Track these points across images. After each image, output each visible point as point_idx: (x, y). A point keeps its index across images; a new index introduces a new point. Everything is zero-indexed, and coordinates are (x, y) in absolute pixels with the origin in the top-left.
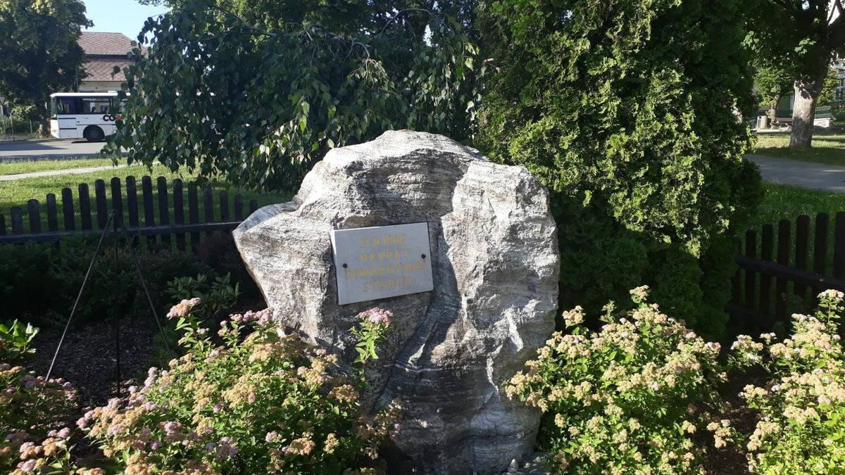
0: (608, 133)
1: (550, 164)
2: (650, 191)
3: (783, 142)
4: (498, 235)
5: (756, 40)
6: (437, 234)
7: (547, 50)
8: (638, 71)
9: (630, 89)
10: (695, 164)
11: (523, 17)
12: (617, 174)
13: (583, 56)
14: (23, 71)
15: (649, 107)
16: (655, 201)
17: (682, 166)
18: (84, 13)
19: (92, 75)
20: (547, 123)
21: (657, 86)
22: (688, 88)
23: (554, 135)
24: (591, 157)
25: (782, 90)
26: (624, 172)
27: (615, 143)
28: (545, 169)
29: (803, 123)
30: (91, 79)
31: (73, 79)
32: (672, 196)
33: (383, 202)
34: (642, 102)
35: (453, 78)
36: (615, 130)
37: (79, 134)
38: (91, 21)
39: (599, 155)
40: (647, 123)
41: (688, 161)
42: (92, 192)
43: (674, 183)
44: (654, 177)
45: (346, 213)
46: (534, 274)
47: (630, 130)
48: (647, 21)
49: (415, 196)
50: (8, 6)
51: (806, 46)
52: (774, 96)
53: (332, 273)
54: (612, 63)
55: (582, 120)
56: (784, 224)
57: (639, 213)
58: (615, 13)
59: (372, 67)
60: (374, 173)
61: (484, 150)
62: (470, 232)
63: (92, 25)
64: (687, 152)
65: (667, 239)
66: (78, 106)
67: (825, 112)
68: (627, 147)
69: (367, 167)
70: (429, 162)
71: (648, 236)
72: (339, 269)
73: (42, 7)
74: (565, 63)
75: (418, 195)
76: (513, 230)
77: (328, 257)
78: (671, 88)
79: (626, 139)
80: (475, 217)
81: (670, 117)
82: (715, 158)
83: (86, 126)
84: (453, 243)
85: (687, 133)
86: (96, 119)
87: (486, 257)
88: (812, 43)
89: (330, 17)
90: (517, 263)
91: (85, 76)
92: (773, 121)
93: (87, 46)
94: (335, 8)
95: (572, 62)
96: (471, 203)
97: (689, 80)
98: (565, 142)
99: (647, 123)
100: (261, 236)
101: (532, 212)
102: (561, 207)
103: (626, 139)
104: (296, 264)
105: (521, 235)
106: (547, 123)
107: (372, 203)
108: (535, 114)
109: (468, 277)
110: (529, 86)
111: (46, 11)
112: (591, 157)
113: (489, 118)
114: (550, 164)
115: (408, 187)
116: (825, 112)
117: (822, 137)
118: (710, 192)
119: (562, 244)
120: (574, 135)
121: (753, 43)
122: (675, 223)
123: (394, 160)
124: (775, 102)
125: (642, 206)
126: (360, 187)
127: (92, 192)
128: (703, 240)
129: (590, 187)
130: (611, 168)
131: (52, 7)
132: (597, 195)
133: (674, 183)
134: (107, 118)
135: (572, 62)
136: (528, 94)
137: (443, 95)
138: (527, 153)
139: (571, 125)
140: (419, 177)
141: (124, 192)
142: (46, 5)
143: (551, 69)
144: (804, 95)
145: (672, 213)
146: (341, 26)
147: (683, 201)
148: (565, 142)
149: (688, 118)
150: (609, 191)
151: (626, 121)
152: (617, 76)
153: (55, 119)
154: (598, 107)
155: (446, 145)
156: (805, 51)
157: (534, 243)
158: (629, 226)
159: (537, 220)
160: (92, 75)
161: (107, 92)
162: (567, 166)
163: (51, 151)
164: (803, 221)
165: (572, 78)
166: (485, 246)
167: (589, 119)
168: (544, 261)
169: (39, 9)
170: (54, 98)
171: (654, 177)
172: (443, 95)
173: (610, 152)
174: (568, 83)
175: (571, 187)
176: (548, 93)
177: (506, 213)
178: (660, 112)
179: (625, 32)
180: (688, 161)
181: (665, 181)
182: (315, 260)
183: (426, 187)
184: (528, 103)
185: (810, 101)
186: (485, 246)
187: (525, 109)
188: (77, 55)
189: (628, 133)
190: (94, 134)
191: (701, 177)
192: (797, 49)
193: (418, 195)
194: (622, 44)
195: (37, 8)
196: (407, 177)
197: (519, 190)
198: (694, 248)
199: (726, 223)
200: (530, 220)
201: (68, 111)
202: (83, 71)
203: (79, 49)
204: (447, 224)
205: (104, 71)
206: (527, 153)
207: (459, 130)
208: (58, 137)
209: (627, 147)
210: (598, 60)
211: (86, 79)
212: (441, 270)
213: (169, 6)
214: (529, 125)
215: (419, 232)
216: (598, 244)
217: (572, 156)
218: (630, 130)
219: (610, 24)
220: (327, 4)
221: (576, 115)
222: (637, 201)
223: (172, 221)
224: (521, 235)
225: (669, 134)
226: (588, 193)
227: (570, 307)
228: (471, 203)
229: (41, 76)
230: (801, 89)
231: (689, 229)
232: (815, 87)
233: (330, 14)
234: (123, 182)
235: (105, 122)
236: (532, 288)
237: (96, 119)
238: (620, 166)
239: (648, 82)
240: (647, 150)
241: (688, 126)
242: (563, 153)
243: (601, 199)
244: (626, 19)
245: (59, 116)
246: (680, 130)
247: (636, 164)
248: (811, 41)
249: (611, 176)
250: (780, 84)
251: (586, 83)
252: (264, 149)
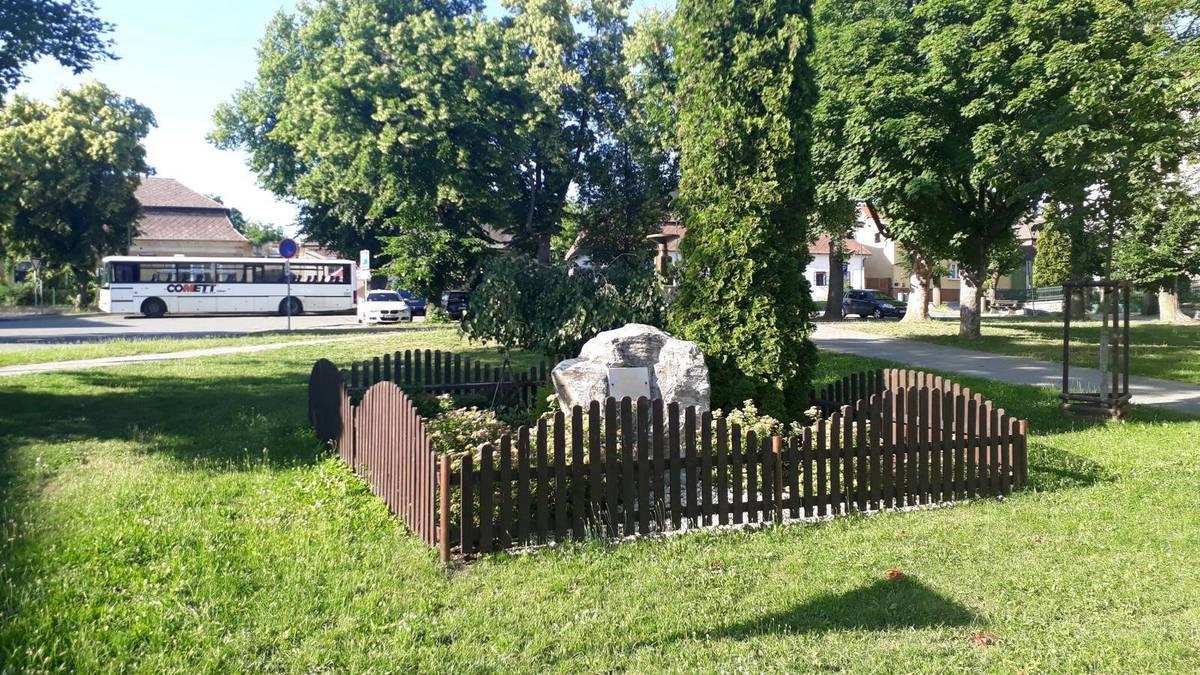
0: (734, 326)
1: (706, 342)
2: (756, 355)
3: (955, 329)
4: (683, 372)
5: (915, 232)
6: (652, 373)
7: (703, 285)
8: (748, 295)
9: (744, 305)
10: (776, 342)
11: (692, 269)
12: (739, 347)
13: (720, 290)
14: (64, 230)
15: (753, 314)
16: (758, 360)
17: (769, 343)
18: (144, 158)
19: (145, 233)
20: (704, 321)
21: (757, 304)
22: (772, 306)
23: (708, 327)
24: (726, 339)
25: (1001, 268)
26: (742, 346)
27: (737, 331)
28: (704, 344)
29: (970, 311)
30: (143, 237)
31: (121, 239)
32: (766, 358)
33: (628, 356)
34: (750, 312)
35: (653, 295)
36: (738, 325)
37: (136, 308)
38: (154, 169)
39: (730, 338)
40: (753, 322)
41: (773, 341)
42: (423, 358)
43: (767, 352)
44: (757, 348)
45: (612, 362)
46: (698, 393)
47: (745, 325)
48: (750, 274)
49: (642, 355)
50: (57, 150)
51: (960, 239)
52: (992, 274)
53: (608, 386)
54: (735, 293)
55: (721, 320)
56: (854, 376)
57: (751, 367)
58: (735, 270)
59: (609, 289)
60: (623, 344)
61: (673, 334)
62: (668, 372)
63: (155, 173)
64: (772, 337)
65: (766, 381)
66: (130, 274)
67: (1054, 293)
68: (743, 333)
69: (621, 341)
70: (649, 339)
71: (755, 379)
72: (611, 386)
73: (101, 152)
74: (712, 292)
75: (643, 354)
76: (688, 371)
77: (606, 380)
78: (764, 305)
79: (742, 329)
80: (670, 365)
81: (763, 319)
82: (787, 339)
83: (143, 299)
84: (659, 376)
85: (772, 327)
86: (158, 290)
87: (676, 384)
88: (965, 237)
89: (470, 182)
90: (690, 387)
91: (137, 234)
92: (992, 303)
93: (144, 196)
94: (475, 171)
95: (715, 292)
96: (669, 358)
97: (773, 302)
98: (713, 330)
99: (753, 322)
100: (574, 371)
101: (697, 362)
102: (711, 362)
103: (742, 329)
104: (592, 383)
105: (692, 374)
106: (704, 321)
107: (624, 357)
108: (698, 316)
109: (667, 393)
110: (694, 302)
111: (104, 157)
112: (726, 339)
113: (674, 317)
114: (706, 342)
115: (639, 350)
116: (1054, 293)
117: (1012, 324)
118: (785, 356)
119: (711, 379)
120: (717, 327)
121: (912, 235)
122: (769, 372)
123: (633, 338)
124: (994, 280)
125: (752, 363)
126: (618, 349)
127: (423, 358)
128: (784, 381)
129: (727, 353)
130: (736, 344)
131: (113, 153)
132: (730, 357)
133: (767, 352)
134: (172, 288)
135: (715, 292)
136: (694, 306)
137: (648, 304)
138: (694, 336)
139: (715, 322)
140: (644, 346)
141: (413, 358)
142: (105, 150)
143: (706, 295)
144: (969, 284)
145: (767, 366)
146: (483, 191)
147: (772, 360)
148: (713, 330)
149: (773, 320)
150: (736, 356)
151: (742, 321)
152: (737, 299)
153: (107, 288)
154: (729, 314)
155: (654, 331)
156: (959, 243)
157: (698, 378)
158: (747, 374)
159: (699, 366)
160: (145, 233)
161: (171, 254)
162: (714, 342)
163: (837, 336)
164: (862, 375)
165: (715, 299)
166: (675, 378)
167: (724, 319)
168: (703, 386)
169: (97, 154)
170: (107, 264)
171: (757, 348)
172: (648, 304)
173: (735, 336)
174: (714, 302)
175: (717, 353)
176: (704, 306)
177: (685, 363)
178: (759, 317)
179: (741, 279)
180: (773, 341)
181: (762, 351)
182: (601, 381)
183: (647, 351)
184: (694, 311)
185: (975, 289)
186: (675, 378)
187: (693, 314)
188: (134, 210)
189: (744, 327)
190: (154, 308)
191: (779, 348)
192: (952, 242)
193: (643, 354)
194: (739, 284)
195: (94, 153)
196: (639, 345)
197: (690, 352)
198: (780, 385)
199: (794, 372)
200: (696, 366)
201: (120, 280)
202: (134, 229)
203: (134, 201)
204: (657, 367)
205: (152, 227)
206: (694, 336)
207: (657, 320)
208: (108, 311)
209: (743, 333)
210: (728, 291)
211: (139, 238)
212: (654, 389)
213: (250, 151)
214: (695, 321)
215: (644, 371)
216: (731, 382)
217: (717, 337)
218: (745, 325)
219: (733, 275)
220: (468, 168)
221: (718, 318)
222: (749, 361)
223: (443, 382)
224: (692, 374)
225: (763, 328)
226: (725, 357)
227: (715, 410)
228: (669, 358)
229: (85, 234)
230: (965, 277)
231: (776, 375)
232: (978, 276)
233: (470, 178)
234: (413, 352)
235: (168, 293)
236: (697, 400)
237: (158, 290)
238: (741, 343)
239: (753, 302)
240: (753, 335)
241: (772, 324)
242: (712, 336)
243: (732, 359)
244: (741, 273)
245: (112, 285)
246: (769, 325)
247: (748, 343)
248: (964, 234)
249: (736, 347)
250: (998, 260)
251: (721, 302)
252: (562, 332)
